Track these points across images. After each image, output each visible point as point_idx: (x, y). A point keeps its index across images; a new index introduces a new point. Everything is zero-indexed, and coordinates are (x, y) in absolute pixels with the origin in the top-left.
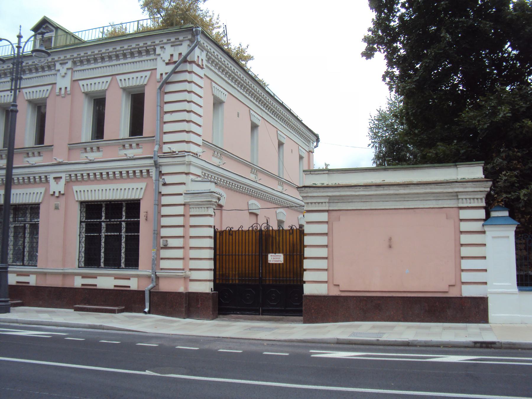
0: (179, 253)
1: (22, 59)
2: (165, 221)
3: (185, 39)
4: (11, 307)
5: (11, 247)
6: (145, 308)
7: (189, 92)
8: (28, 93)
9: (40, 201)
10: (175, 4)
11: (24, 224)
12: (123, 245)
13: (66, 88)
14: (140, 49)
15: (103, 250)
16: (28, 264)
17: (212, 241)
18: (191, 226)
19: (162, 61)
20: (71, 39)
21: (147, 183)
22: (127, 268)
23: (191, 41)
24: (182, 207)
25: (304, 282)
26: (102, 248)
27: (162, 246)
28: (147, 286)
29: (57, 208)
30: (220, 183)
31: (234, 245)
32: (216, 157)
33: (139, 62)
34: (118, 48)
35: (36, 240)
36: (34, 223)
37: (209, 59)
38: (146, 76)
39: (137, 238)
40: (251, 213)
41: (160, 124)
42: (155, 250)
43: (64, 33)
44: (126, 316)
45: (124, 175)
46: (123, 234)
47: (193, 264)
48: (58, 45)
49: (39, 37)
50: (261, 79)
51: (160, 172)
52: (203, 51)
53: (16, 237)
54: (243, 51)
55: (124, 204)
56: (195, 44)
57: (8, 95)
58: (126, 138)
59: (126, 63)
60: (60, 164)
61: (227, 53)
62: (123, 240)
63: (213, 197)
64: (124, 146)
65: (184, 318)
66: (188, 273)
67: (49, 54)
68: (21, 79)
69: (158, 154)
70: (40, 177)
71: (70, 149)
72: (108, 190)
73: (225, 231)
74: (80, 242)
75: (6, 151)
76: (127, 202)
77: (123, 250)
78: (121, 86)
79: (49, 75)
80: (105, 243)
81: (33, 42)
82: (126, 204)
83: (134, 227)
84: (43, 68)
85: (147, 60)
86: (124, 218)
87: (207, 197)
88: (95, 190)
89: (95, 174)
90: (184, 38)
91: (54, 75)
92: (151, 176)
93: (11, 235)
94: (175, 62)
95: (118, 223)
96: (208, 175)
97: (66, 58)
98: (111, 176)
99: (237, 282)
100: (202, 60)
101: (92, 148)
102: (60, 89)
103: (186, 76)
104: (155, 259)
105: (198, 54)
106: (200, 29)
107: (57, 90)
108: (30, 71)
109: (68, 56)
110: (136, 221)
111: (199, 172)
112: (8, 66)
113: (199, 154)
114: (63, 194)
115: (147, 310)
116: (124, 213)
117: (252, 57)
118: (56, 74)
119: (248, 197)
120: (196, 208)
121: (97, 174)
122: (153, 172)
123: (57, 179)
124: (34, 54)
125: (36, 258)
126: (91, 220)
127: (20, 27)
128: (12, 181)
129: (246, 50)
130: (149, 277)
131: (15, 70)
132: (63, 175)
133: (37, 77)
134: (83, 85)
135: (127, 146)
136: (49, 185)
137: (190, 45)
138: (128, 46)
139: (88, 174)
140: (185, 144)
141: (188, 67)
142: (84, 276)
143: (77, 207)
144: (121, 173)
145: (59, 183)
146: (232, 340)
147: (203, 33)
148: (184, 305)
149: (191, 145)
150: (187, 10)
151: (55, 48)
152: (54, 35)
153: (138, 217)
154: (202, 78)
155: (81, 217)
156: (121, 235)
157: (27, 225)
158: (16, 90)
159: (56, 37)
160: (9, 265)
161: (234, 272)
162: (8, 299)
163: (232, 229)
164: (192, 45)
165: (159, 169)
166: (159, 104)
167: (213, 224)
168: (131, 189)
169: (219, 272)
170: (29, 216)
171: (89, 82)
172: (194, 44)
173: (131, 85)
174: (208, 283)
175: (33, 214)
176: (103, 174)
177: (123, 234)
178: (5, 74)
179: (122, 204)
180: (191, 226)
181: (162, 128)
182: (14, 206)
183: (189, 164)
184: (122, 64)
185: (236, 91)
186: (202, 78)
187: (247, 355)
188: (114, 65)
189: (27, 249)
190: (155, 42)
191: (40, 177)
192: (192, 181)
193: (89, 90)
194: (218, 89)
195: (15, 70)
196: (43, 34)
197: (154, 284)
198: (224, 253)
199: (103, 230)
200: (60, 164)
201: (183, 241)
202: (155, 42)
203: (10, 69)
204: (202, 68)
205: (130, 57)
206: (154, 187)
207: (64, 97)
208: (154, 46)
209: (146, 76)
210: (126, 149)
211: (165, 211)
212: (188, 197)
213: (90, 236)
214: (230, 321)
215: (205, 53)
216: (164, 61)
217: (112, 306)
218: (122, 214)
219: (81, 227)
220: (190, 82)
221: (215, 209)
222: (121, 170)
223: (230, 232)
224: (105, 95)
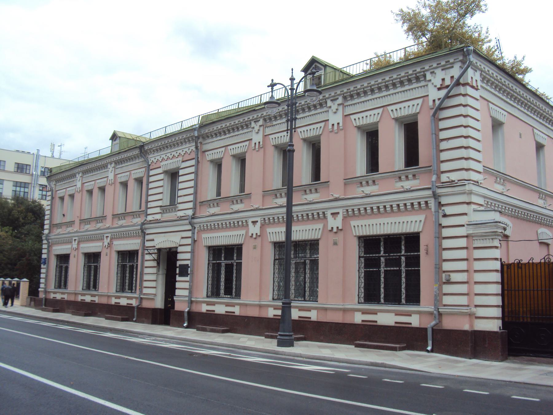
0: (463, 289)
1: (295, 100)
2: (446, 255)
3: (456, 61)
4: (294, 341)
5: (292, 283)
6: (427, 346)
7: (465, 116)
8: (302, 132)
9: (319, 237)
10: (439, 24)
11: (305, 260)
12: (403, 280)
13: (338, 124)
14: (409, 77)
15: (382, 286)
16: (309, 299)
17: (499, 275)
18: (476, 260)
19: (433, 86)
20: (339, 75)
21: (426, 216)
22: (415, 305)
23: (463, 62)
24: (465, 239)
25: (176, 289)
26: (381, 284)
27: (444, 281)
28: (430, 323)
29: (335, 244)
30: (505, 212)
31: (531, 279)
32: (499, 183)
33: (409, 90)
34: (387, 78)
35: (316, 275)
36: (314, 259)
37: (483, 79)
38: (418, 104)
39: (418, 273)
40: (541, 243)
41: (436, 152)
42: (437, 285)
43: (332, 70)
44: (408, 355)
45: (402, 208)
46: (403, 269)
47: (479, 300)
48: (327, 82)
49: (309, 77)
50: (542, 93)
51: (440, 203)
52: (476, 71)
53: (297, 272)
54: (519, 64)
55: (403, 237)
56: (468, 65)
57: (284, 136)
58: (402, 169)
59: (397, 93)
60: (336, 200)
61: (501, 69)
62: (403, 275)
63: (498, 227)
64: (400, 178)
65: (470, 359)
66: (474, 309)
67: (320, 93)
68: (296, 119)
69: (436, 184)
70: (318, 214)
71: (345, 184)
72: (386, 224)
73: (513, 264)
74: (359, 278)
75: (286, 190)
76: (405, 236)
77: (403, 286)
78: (393, 117)
79: (321, 113)
80: (384, 278)
81: (303, 82)
82: (405, 237)
83: (414, 261)
84: (315, 106)
85: (418, 88)
86: (403, 253)
87: (492, 228)
88: (373, 225)
89: (372, 208)
90: (455, 60)
91: (326, 112)
92: (430, 207)
93: (293, 271)
94: (447, 87)
95: (398, 257)
96: (491, 203)
97: (336, 94)
98: (388, 209)
99: (529, 320)
100: (476, 81)
101: (367, 182)
102: (333, 125)
103: (461, 100)
104: (437, 295)
105: (472, 76)
106: (472, 48)
107: (330, 127)
108: (303, 110)
109: (339, 92)
110: (368, 256)
111: (481, 201)
112: (283, 108)
113: (480, 182)
114: (341, 230)
115: (429, 348)
116: (403, 247)
117: (530, 69)
118: (328, 111)
119: (537, 225)
120: (480, 239)
121: (374, 208)
122: (432, 203)
123: (254, 223)
124: (306, 94)
125: (316, 294)
126: (411, 253)
127: (292, 70)
128: (293, 218)
129: (522, 63)
130: (431, 313)
131: (289, 110)
132: (340, 211)
133: (310, 115)
134: (355, 119)
135: (403, 177)
136: (249, 228)
137: (463, 66)
138: (397, 75)
139: (365, 209)
140: (464, 172)
141: (462, 90)
142: (364, 312)
143: (356, 242)
144: (405, 205)
145: (337, 218)
146: (526, 386)
147: (475, 52)
148: (470, 345)
149: (471, 172)
150: (453, 29)
151: (324, 86)
152: (323, 73)
153: (418, 251)
154: (477, 100)
155: (359, 252)
156: (401, 270)
157: (307, 261)
158: (291, 130)
159: (325, 74)
160: (292, 300)
161: (525, 309)
162: (292, 333)
163: (521, 262)
164: (464, 66)
165: (438, 200)
166: (434, 132)
167: (499, 257)
168: (409, 223)
169: (508, 308)
170: (309, 252)
171: (360, 115)
172: (466, 65)
173: (403, 114)
174: (496, 320)
175: (313, 251)
176: (386, 207)
177: (403, 269)
178: (281, 116)
179: (400, 238)
180: (476, 260)
181: (438, 157)
182: (294, 243)
183: (470, 193)
184: (393, 94)
185: (517, 110)
186: (477, 100)
187: (338, 375)
188: (384, 96)
189: (307, 285)
190: (424, 68)
191: (318, 214)
192: (475, 211)
193: (361, 124)
194: (496, 110)
195: (289, 110)
196: (313, 73)
197: (437, 321)
198: (513, 289)
199: (383, 265)
200: (336, 200)
201: (467, 276)
202: (424, 68)
203: (285, 111)
204: (477, 89)
205: (392, 89)
206: (434, 220)
207: (337, 133)
208: (424, 72)
209: (418, 104)
210: (402, 181)
211: (446, 244)
212: (471, 228)
213: (369, 271)
214: (522, 364)
215: (478, 73)
216: (435, 86)
217: (393, 343)
218: (401, 248)
219: (360, 262)
220: (465, 106)
221: (501, 240)
222: (398, 203)
223: (519, 265)
224: (378, 127)
